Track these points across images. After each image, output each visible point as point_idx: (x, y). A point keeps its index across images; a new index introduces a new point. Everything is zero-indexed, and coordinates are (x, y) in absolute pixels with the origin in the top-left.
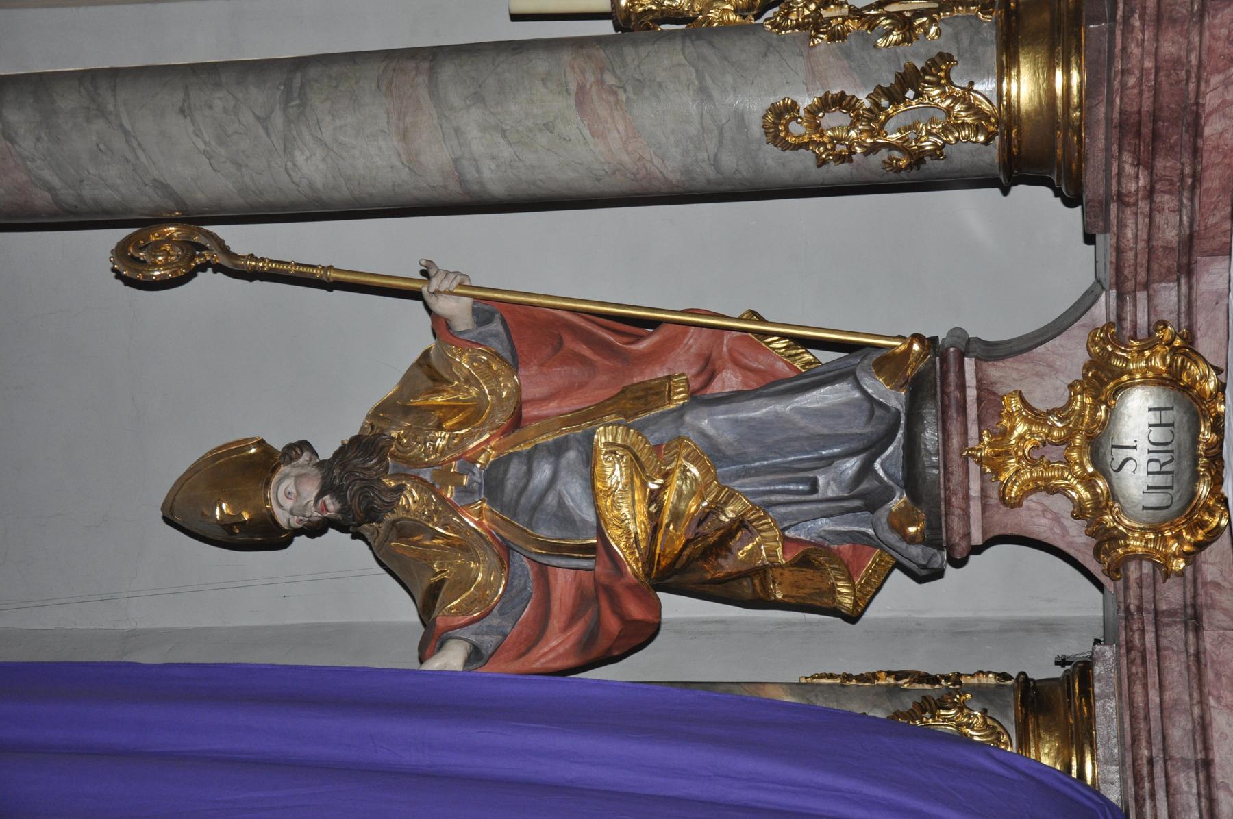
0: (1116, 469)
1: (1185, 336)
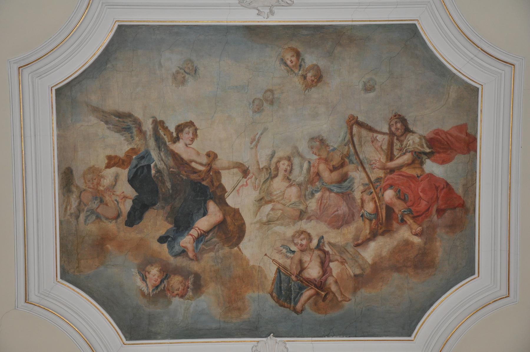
0: (504, 72)
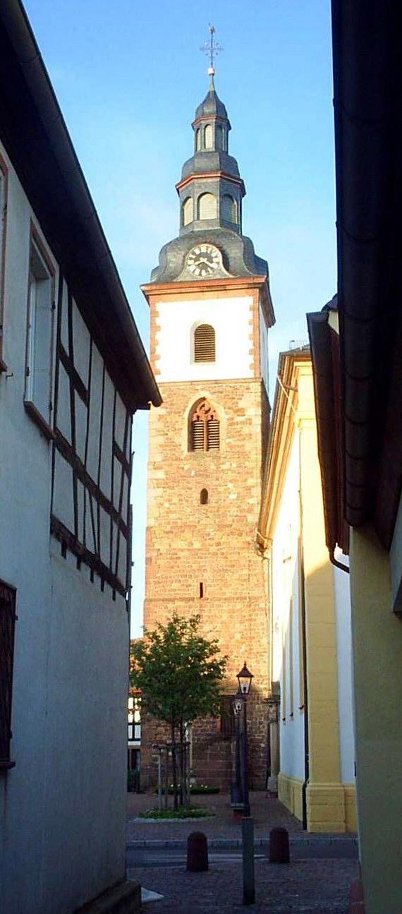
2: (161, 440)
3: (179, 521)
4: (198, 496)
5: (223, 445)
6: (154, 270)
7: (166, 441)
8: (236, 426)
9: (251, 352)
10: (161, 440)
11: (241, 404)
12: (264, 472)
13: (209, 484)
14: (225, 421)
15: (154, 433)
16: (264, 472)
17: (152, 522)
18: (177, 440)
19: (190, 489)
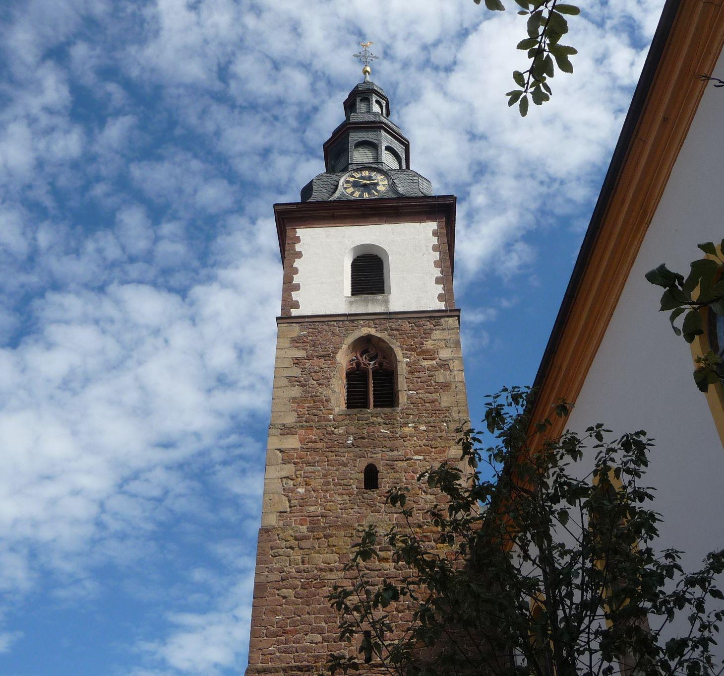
1: (583, 500)
2: (296, 392)
3: (322, 520)
4: (357, 476)
5: (403, 398)
6: (277, 204)
7: (304, 394)
8: (421, 374)
9: (438, 281)
10: (296, 392)
11: (429, 344)
12: (556, 378)
13: (379, 458)
14: (404, 365)
15: (285, 382)
16: (556, 378)
17: (273, 520)
18: (324, 392)
19: (345, 465)
